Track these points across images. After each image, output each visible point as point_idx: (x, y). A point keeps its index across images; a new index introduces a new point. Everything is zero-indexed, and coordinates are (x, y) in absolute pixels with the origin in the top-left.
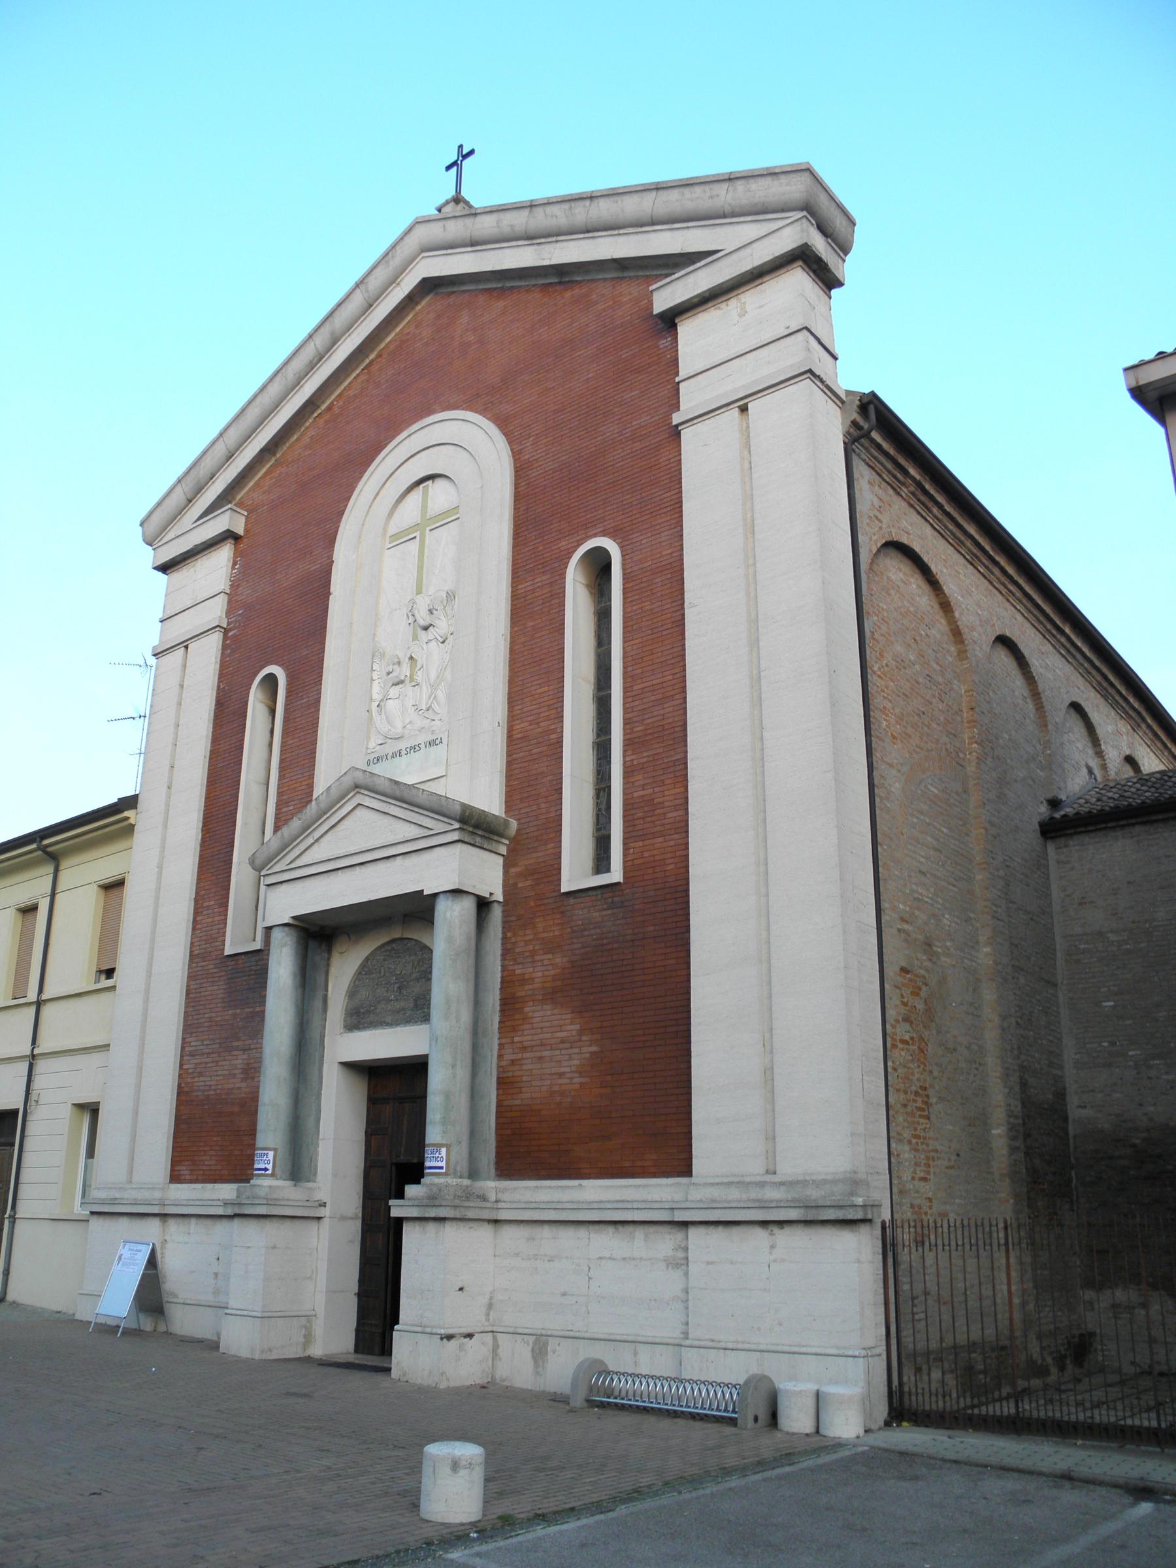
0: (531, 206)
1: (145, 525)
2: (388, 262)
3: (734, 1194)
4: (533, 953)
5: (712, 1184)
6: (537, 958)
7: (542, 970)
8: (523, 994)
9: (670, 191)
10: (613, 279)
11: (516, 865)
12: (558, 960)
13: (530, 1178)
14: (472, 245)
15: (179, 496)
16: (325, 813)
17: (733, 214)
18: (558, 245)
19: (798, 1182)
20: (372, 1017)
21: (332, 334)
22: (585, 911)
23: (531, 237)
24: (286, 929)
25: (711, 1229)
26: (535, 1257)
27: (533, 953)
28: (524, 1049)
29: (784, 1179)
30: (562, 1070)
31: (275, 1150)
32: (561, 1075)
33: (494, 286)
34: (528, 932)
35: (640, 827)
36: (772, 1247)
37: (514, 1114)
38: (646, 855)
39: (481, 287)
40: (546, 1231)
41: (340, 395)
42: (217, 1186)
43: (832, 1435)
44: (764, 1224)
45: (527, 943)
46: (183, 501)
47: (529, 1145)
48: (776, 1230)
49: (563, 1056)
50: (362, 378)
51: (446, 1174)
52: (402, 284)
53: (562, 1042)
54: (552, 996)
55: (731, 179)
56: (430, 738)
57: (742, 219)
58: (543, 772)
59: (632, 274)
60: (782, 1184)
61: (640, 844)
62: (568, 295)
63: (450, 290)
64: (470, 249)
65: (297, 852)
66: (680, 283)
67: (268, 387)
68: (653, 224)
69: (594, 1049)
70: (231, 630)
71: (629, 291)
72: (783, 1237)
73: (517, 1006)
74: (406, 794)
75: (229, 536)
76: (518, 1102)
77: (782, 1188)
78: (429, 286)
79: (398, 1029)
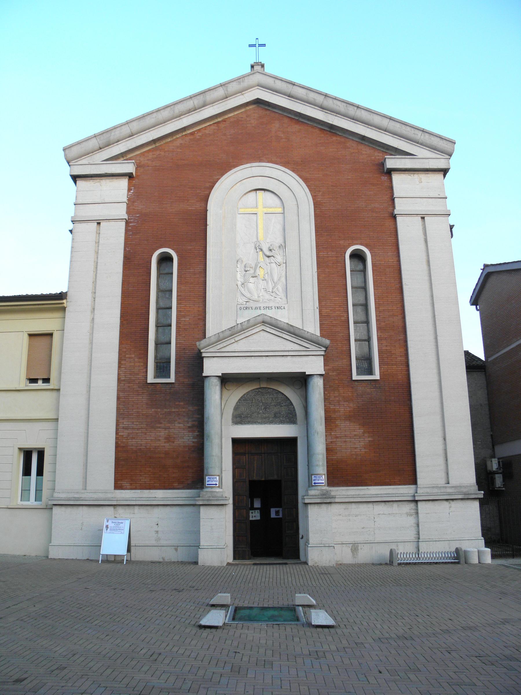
0: (326, 96)
1: (67, 151)
2: (240, 83)
3: (435, 491)
4: (339, 401)
5: (427, 488)
6: (341, 403)
7: (344, 408)
8: (335, 416)
9: (397, 123)
10: (357, 141)
11: (328, 366)
12: (351, 405)
13: (343, 486)
14: (289, 96)
15: (94, 144)
16: (244, 330)
17: (421, 144)
18: (336, 117)
19: (458, 486)
20: (249, 419)
21: (205, 102)
22: (363, 388)
23: (322, 108)
24: (217, 378)
25: (427, 502)
26: (349, 515)
27: (339, 401)
28: (337, 437)
29: (452, 485)
30: (356, 446)
31: (324, 475)
32: (356, 448)
33: (293, 117)
34: (336, 392)
35: (386, 360)
36: (450, 507)
37: (333, 462)
38: (389, 371)
39: (285, 114)
40: (354, 506)
41: (199, 130)
42: (151, 491)
43: (486, 563)
44: (447, 500)
45: (335, 397)
46: (97, 146)
47: (341, 474)
48: (451, 502)
49: (357, 442)
50: (213, 127)
51: (325, 485)
52: (245, 95)
53: (355, 436)
54: (350, 417)
55: (423, 131)
56: (277, 305)
57: (424, 147)
58: (338, 332)
59: (367, 144)
60: (452, 487)
61: (386, 367)
62: (334, 138)
63: (266, 107)
64: (287, 97)
65: (225, 344)
66: (398, 160)
67: (162, 111)
68: (385, 131)
69: (370, 439)
70: (131, 222)
71: (377, 155)
72: (453, 504)
73: (332, 421)
74: (297, 332)
75: (130, 176)
76: (336, 458)
77: (453, 488)
78: (258, 102)
79: (266, 425)
